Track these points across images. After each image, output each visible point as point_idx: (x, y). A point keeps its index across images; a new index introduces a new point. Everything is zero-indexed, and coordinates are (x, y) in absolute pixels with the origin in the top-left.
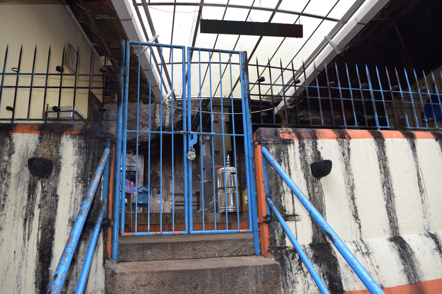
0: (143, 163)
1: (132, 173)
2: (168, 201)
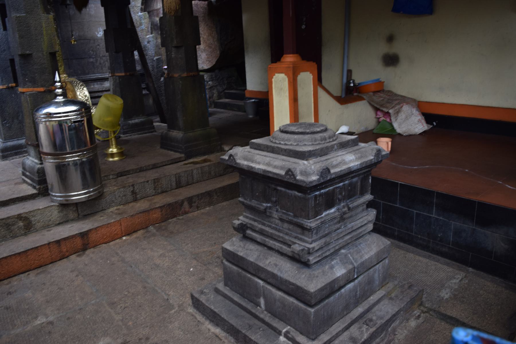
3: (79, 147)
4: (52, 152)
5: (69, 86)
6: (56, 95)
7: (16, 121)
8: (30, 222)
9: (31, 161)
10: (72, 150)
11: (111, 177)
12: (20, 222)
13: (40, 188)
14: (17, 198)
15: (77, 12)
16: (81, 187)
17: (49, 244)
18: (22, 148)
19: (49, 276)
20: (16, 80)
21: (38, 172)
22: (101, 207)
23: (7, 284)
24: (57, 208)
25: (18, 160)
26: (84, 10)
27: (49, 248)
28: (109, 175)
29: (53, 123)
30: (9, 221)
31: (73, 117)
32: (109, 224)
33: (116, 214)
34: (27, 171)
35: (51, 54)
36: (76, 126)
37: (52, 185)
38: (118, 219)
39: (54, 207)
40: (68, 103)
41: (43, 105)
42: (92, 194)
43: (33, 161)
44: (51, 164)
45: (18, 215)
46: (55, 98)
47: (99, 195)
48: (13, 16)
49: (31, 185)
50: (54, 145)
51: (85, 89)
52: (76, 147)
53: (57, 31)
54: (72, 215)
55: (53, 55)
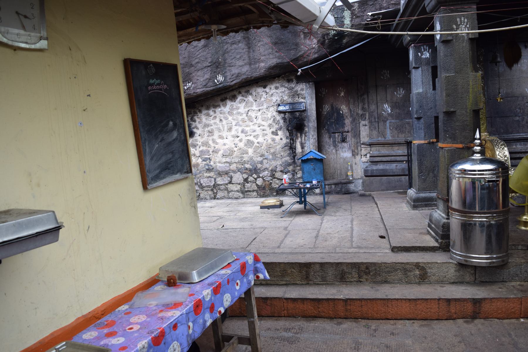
0: (314, 96)
1: (298, 114)
2: (359, 156)
3: (489, 208)
4: (461, 208)
5: (488, 145)
6: (475, 152)
7: (431, 174)
8: (426, 273)
9: (439, 214)
10: (481, 210)
11: (520, 247)
12: (417, 270)
13: (441, 243)
14: (419, 247)
15: (507, 69)
16: (484, 251)
17: (439, 299)
18: (433, 201)
19: (432, 331)
20: (437, 136)
21: (443, 227)
22: (502, 278)
23: (393, 325)
24: (454, 266)
25: (426, 211)
26: (515, 67)
27: (439, 304)
28: (518, 245)
29: (467, 180)
30: (408, 266)
31: (488, 176)
32: (507, 298)
33: (518, 290)
34: (433, 223)
35: (474, 111)
36: (489, 185)
37: (454, 242)
38: (519, 296)
39: (451, 265)
40: (485, 161)
41: (459, 161)
42: (494, 261)
43: (440, 215)
44: (458, 220)
45: (417, 263)
46: (472, 155)
47: (502, 264)
48: (443, 76)
49: (434, 237)
50: (464, 202)
51: (506, 148)
52: (486, 207)
53: (483, 89)
54: (468, 278)
55: (476, 112)
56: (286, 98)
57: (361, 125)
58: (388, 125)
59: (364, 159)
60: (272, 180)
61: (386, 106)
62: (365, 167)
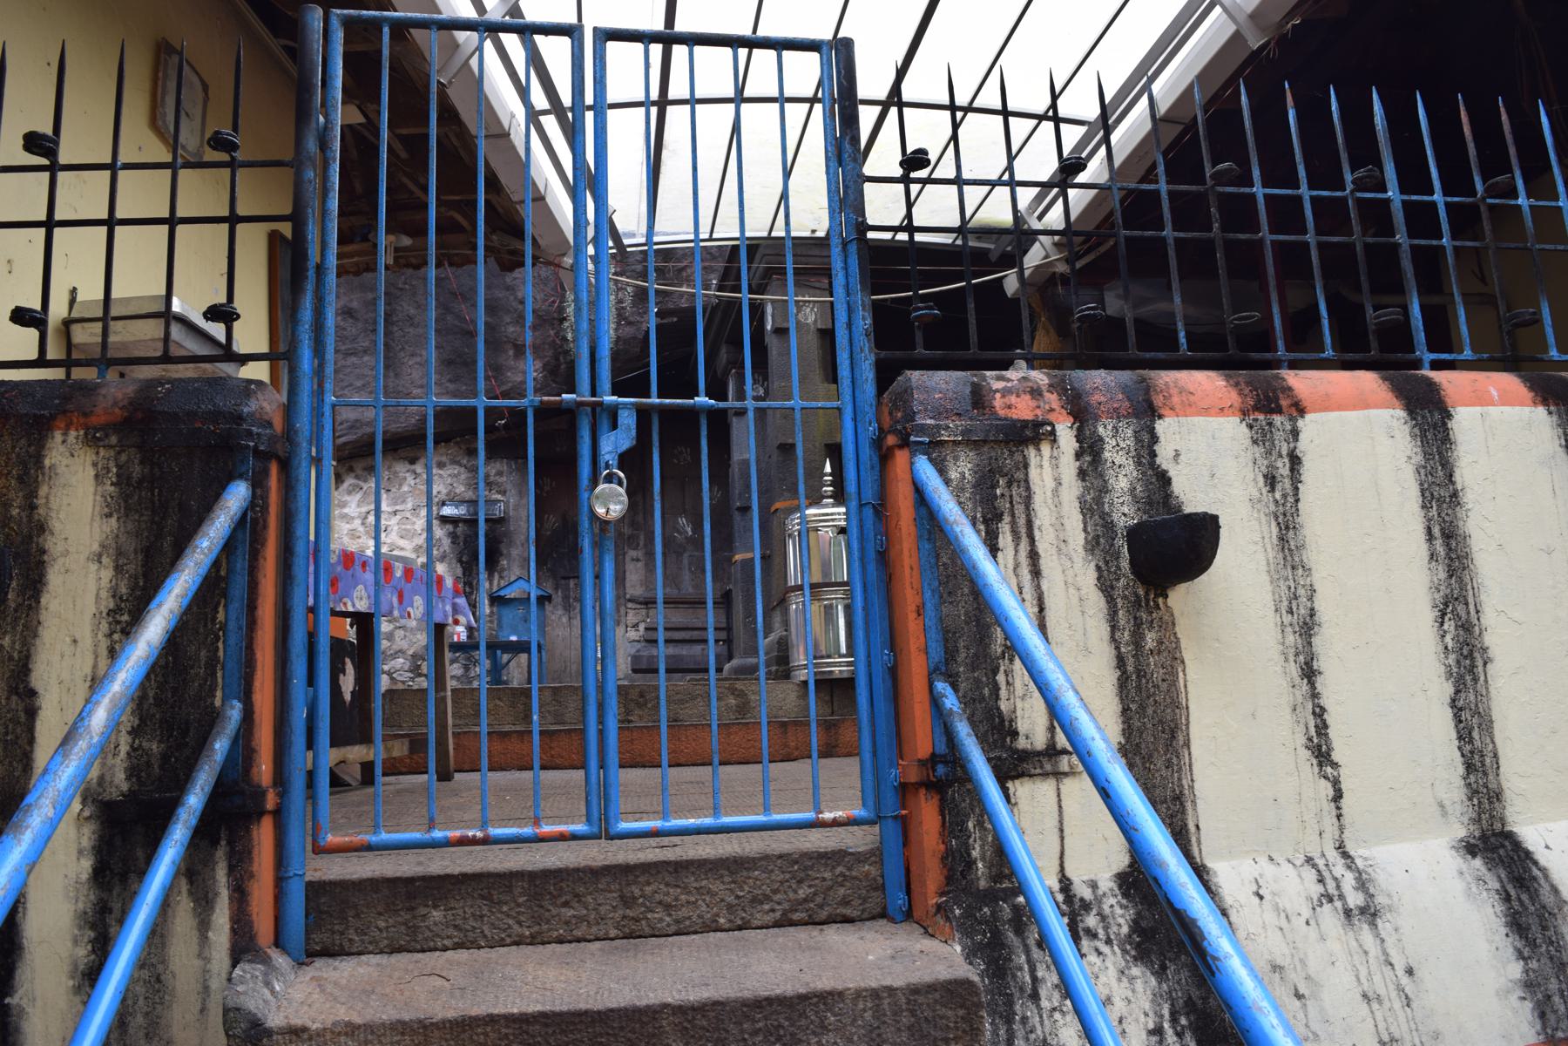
56: (460, 489)
57: (628, 559)
58: (686, 561)
59: (632, 634)
60: (412, 679)
61: (682, 521)
62: (633, 651)
